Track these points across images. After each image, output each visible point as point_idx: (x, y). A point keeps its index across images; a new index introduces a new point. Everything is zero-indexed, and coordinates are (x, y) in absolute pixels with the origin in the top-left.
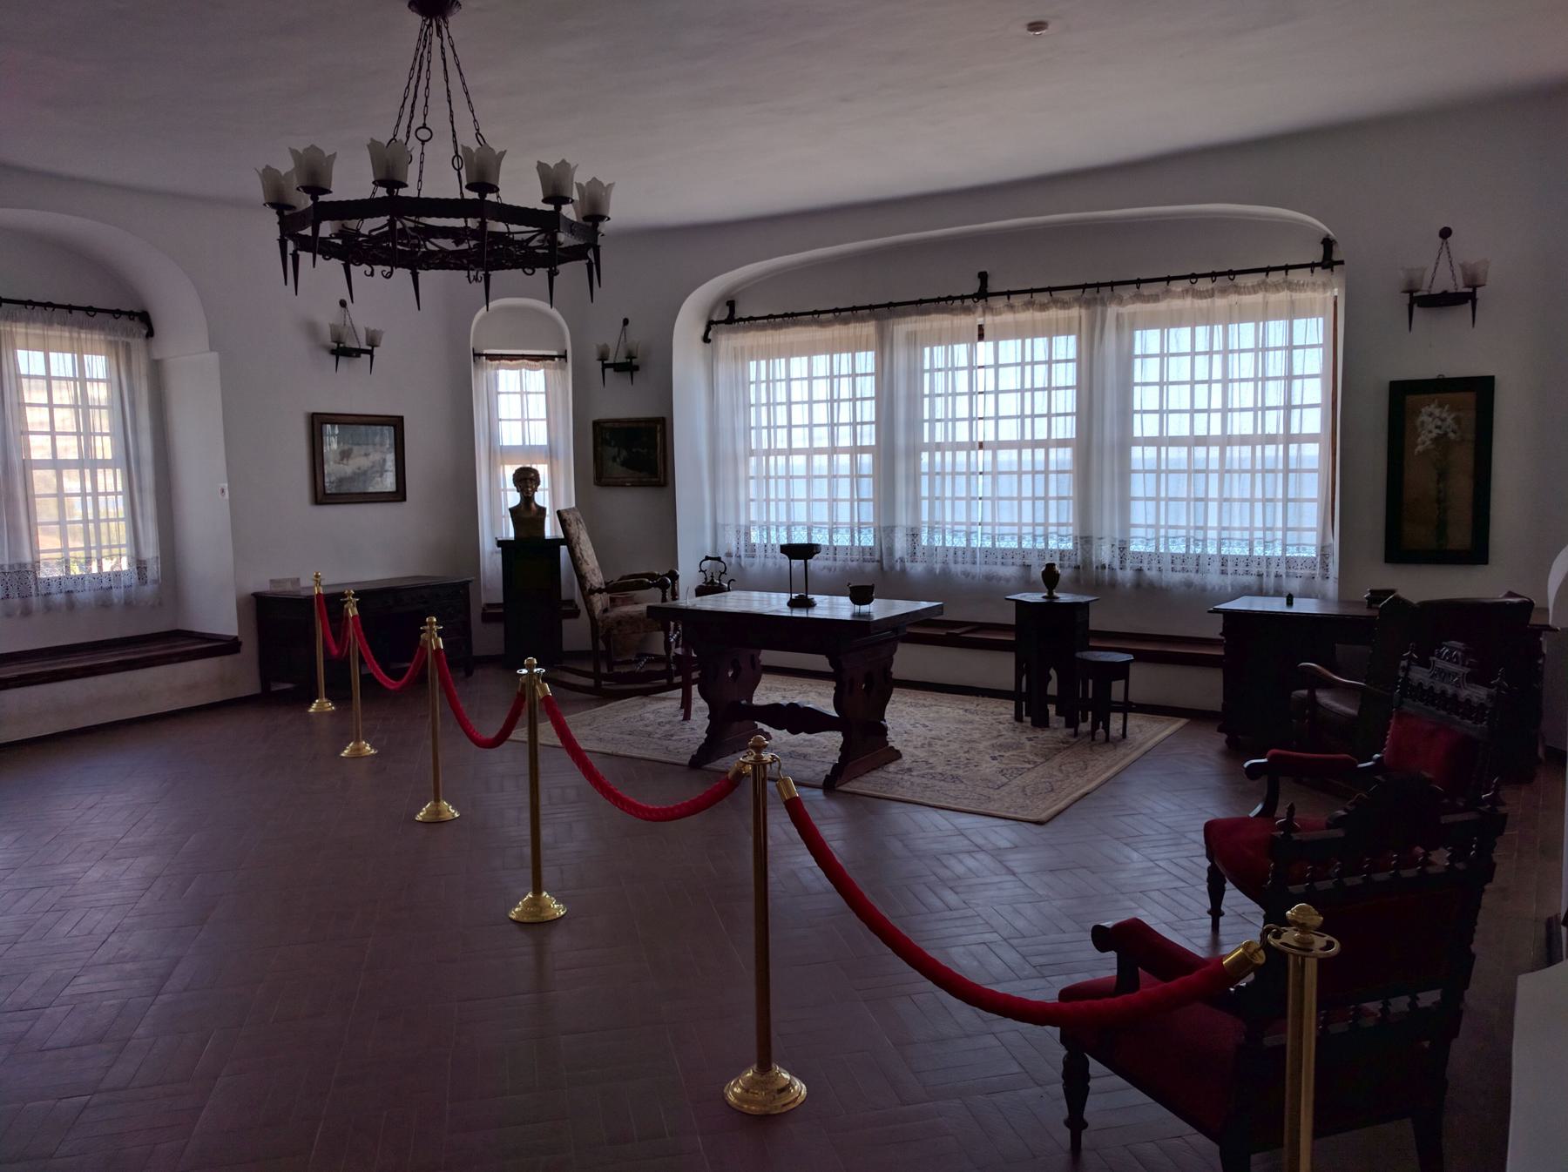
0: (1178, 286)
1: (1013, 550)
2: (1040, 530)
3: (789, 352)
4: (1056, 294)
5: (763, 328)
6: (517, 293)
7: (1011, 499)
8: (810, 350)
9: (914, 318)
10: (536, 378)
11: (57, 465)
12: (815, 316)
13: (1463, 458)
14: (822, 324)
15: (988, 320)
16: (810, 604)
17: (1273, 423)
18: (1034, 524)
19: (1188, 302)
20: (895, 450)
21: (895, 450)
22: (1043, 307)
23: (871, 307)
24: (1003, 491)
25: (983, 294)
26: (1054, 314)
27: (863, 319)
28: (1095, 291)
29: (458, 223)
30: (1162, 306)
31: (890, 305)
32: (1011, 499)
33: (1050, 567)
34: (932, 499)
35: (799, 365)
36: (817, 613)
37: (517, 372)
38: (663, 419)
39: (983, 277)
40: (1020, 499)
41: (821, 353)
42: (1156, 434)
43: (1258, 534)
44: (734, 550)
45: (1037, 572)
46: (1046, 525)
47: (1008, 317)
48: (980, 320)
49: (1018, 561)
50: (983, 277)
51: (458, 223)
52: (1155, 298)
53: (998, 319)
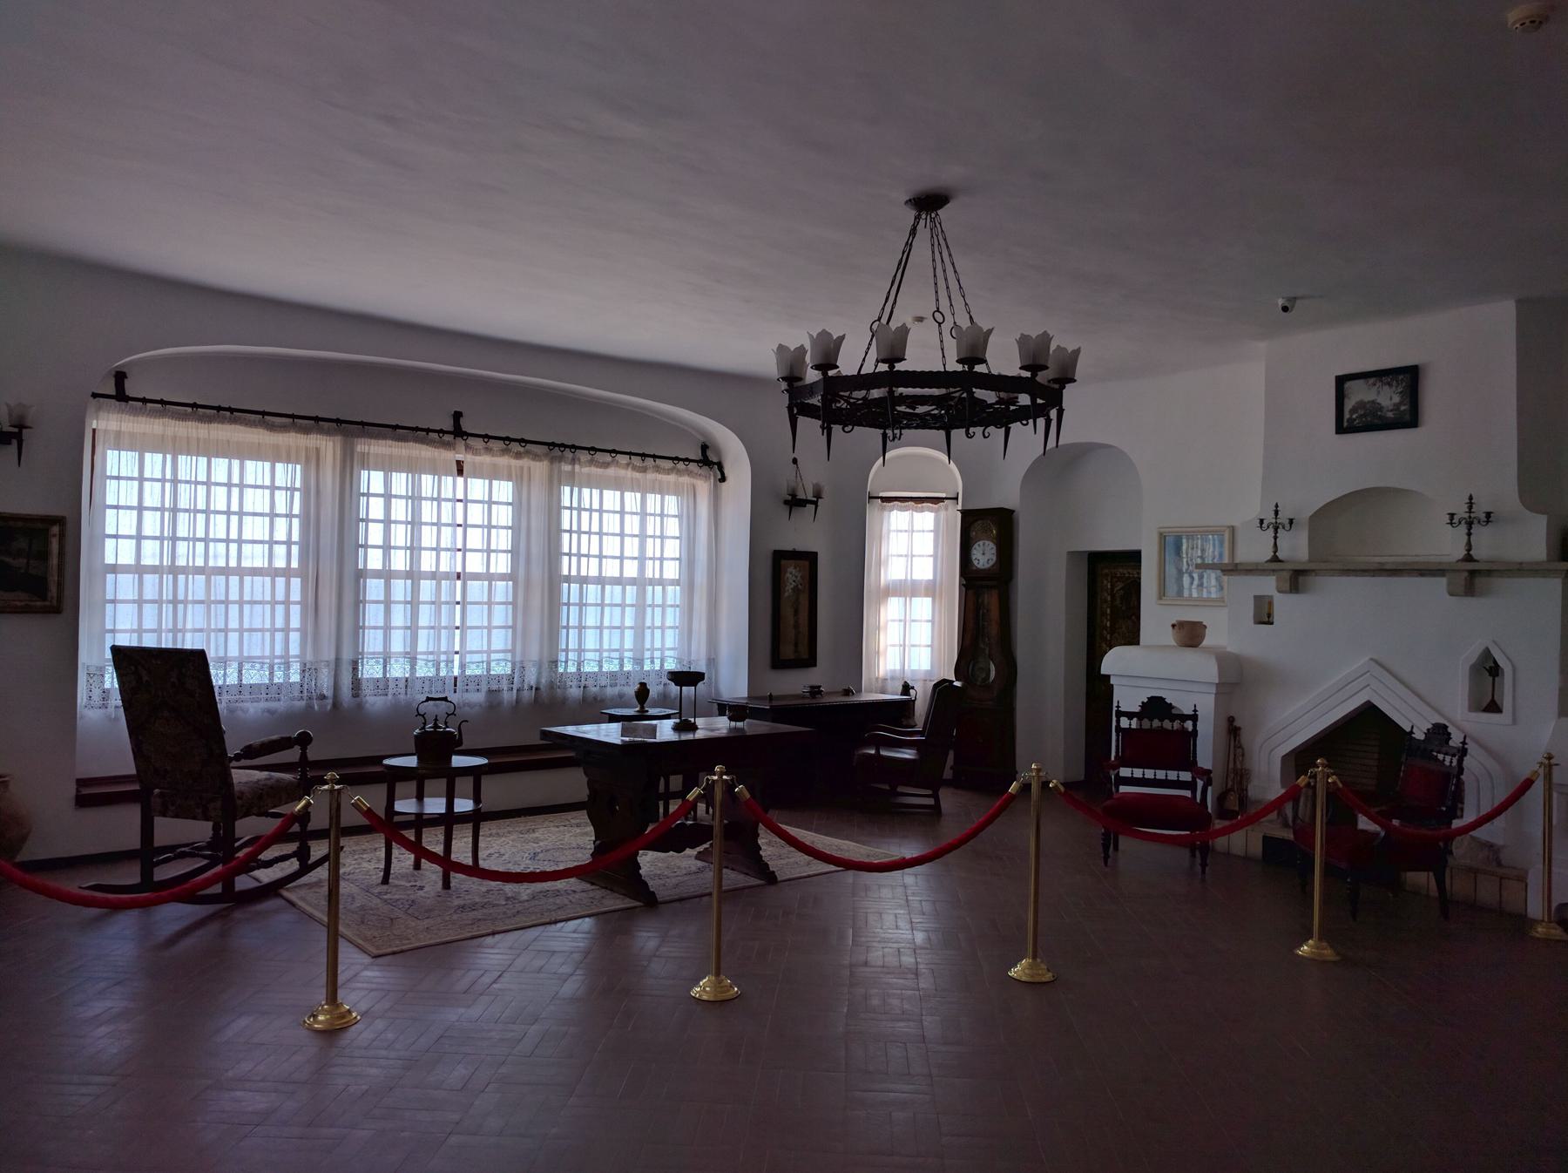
0: (623, 459)
1: (430, 679)
2: (657, 654)
3: (210, 450)
4: (529, 446)
5: (183, 417)
6: (919, 455)
7: (251, 630)
8: (619, 485)
9: (390, 442)
10: (925, 519)
11: (387, 575)
12: (262, 417)
13: (804, 600)
14: (272, 428)
15: (468, 458)
16: (694, 728)
17: (631, 570)
18: (273, 656)
19: (629, 473)
20: (541, 578)
21: (541, 578)
22: (518, 456)
23: (338, 421)
24: (472, 620)
25: (458, 432)
26: (504, 461)
27: (328, 433)
28: (558, 450)
29: (935, 392)
30: (611, 471)
31: (363, 424)
32: (262, 630)
33: (643, 685)
34: (286, 630)
35: (611, 498)
36: (700, 734)
37: (907, 514)
38: (60, 521)
39: (457, 416)
40: (241, 631)
41: (400, 471)
42: (617, 575)
43: (443, 657)
44: (328, 692)
45: (631, 690)
46: (662, 650)
47: (486, 459)
48: (460, 457)
49: (484, 688)
50: (457, 416)
51: (935, 392)
52: (606, 465)
53: (478, 459)
